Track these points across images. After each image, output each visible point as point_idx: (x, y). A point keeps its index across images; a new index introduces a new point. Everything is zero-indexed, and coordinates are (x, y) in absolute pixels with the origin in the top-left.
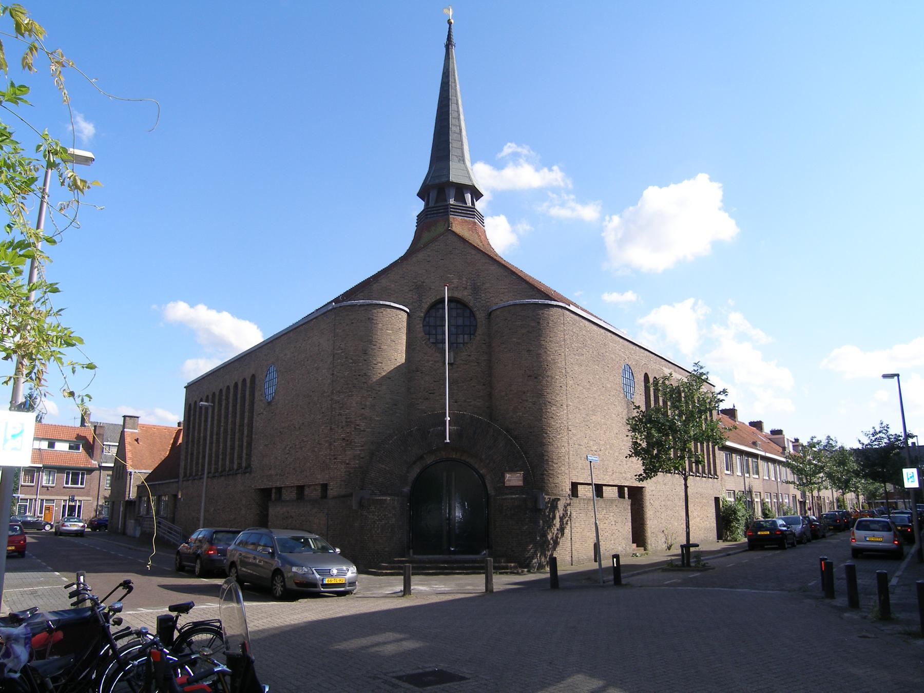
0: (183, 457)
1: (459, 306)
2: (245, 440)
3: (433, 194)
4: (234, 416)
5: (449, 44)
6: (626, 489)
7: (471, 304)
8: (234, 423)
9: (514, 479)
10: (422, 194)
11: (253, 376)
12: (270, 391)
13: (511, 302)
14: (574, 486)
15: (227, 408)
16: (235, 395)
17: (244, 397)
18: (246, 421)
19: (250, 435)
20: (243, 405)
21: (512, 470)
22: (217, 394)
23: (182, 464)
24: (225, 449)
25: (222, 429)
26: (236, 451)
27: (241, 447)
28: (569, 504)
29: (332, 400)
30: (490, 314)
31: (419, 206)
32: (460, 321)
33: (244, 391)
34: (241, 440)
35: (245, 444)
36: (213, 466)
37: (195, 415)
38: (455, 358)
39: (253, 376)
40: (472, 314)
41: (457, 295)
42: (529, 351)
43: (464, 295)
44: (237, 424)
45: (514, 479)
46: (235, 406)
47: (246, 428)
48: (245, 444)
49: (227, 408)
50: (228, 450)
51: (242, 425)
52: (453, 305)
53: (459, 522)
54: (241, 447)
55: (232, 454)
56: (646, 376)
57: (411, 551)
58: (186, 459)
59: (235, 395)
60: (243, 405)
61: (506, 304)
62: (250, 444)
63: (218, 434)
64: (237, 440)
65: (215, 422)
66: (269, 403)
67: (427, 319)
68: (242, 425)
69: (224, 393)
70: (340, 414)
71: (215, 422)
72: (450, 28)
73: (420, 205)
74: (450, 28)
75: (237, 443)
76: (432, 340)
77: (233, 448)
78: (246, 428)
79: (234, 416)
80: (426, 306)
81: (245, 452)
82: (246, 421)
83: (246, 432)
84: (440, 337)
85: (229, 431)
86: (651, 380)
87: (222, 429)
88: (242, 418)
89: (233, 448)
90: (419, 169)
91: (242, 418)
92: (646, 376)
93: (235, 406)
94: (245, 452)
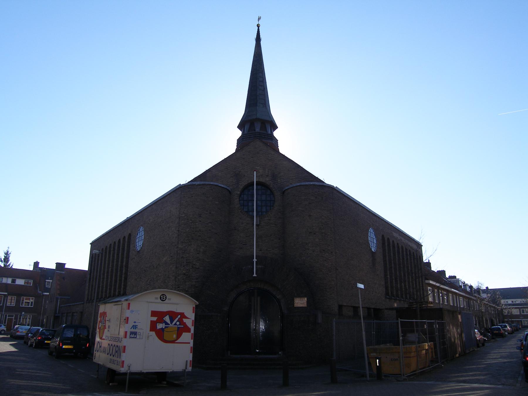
0: (87, 288)
1: (263, 188)
2: (123, 276)
3: (247, 127)
4: (117, 261)
5: (258, 39)
6: (372, 310)
7: (271, 186)
8: (117, 265)
9: (301, 302)
10: (240, 127)
11: (130, 235)
12: (139, 244)
13: (298, 184)
14: (340, 307)
15: (113, 256)
16: (119, 247)
17: (123, 249)
18: (124, 264)
19: (126, 274)
20: (123, 254)
21: (300, 296)
22: (108, 247)
23: (87, 292)
24: (111, 282)
25: (110, 269)
26: (118, 283)
27: (121, 280)
28: (26, 343)
29: (178, 247)
30: (284, 192)
31: (239, 133)
32: (264, 198)
33: (124, 244)
34: (121, 276)
35: (123, 278)
36: (104, 293)
37: (95, 261)
38: (260, 221)
39: (130, 235)
40: (272, 193)
41: (261, 180)
42: (310, 216)
43: (266, 180)
44: (119, 266)
45: (301, 302)
46: (118, 254)
47: (124, 268)
48: (123, 278)
49: (113, 256)
50: (113, 283)
51: (122, 267)
52: (259, 187)
53: (263, 332)
54: (121, 280)
55: (115, 285)
56: (383, 236)
57: (229, 352)
58: (89, 290)
59: (119, 247)
60: (123, 254)
61: (295, 185)
62: (126, 279)
63: (108, 273)
64: (118, 276)
65: (106, 265)
66: (139, 252)
67: (242, 196)
68: (122, 267)
69: (112, 247)
70: (182, 257)
71: (106, 265)
72: (258, 29)
73: (239, 133)
74: (258, 29)
75: (118, 278)
76: (245, 210)
77: (116, 282)
78: (124, 268)
79: (117, 261)
80: (242, 187)
81: (123, 284)
82: (124, 264)
83: (124, 271)
84: (250, 204)
85: (114, 270)
86: (386, 239)
87: (110, 269)
88: (122, 262)
89: (116, 282)
90: (239, 110)
91: (122, 262)
92: (383, 236)
93: (118, 254)
94: (123, 284)
